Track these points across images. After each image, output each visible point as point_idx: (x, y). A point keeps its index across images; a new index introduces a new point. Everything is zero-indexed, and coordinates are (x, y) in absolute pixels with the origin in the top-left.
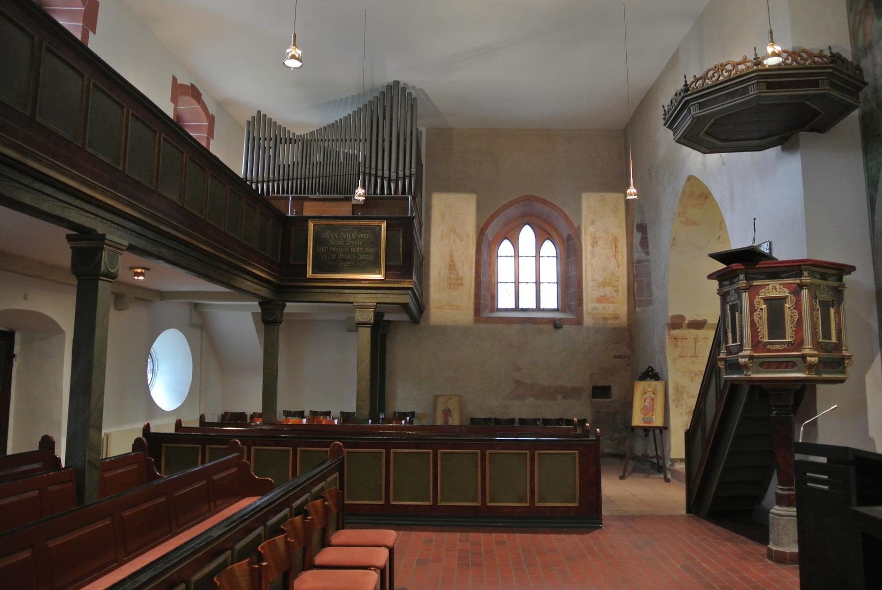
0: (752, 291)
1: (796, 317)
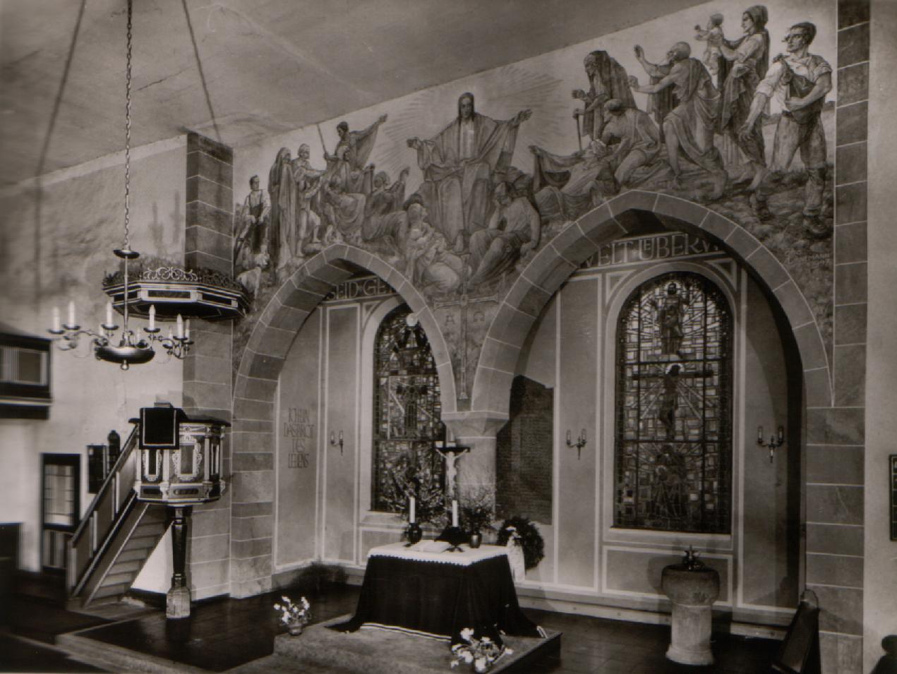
1: (201, 459)
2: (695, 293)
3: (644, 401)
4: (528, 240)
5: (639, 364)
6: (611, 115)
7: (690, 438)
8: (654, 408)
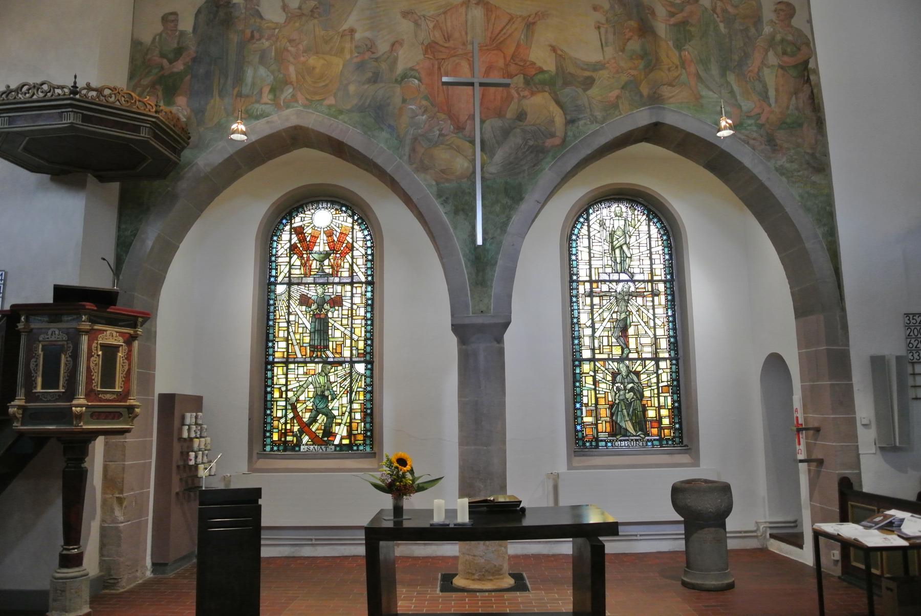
0: (93, 334)
1: (126, 368)
2: (640, 217)
3: (598, 319)
4: (553, 135)
5: (591, 282)
6: (631, 34)
7: (644, 356)
8: (609, 325)
